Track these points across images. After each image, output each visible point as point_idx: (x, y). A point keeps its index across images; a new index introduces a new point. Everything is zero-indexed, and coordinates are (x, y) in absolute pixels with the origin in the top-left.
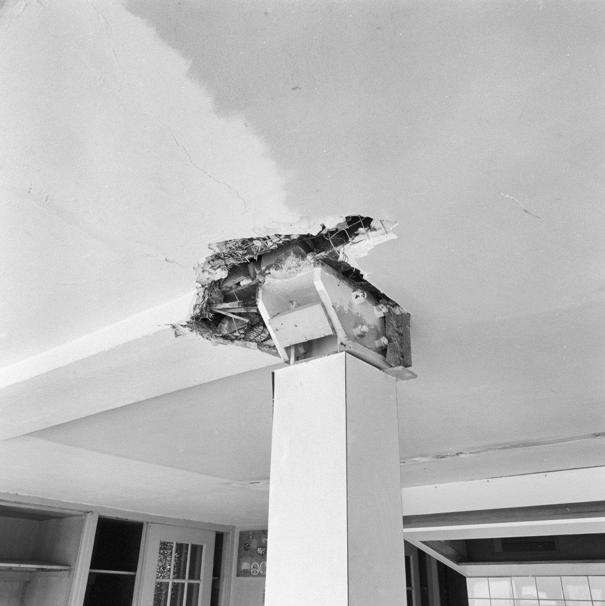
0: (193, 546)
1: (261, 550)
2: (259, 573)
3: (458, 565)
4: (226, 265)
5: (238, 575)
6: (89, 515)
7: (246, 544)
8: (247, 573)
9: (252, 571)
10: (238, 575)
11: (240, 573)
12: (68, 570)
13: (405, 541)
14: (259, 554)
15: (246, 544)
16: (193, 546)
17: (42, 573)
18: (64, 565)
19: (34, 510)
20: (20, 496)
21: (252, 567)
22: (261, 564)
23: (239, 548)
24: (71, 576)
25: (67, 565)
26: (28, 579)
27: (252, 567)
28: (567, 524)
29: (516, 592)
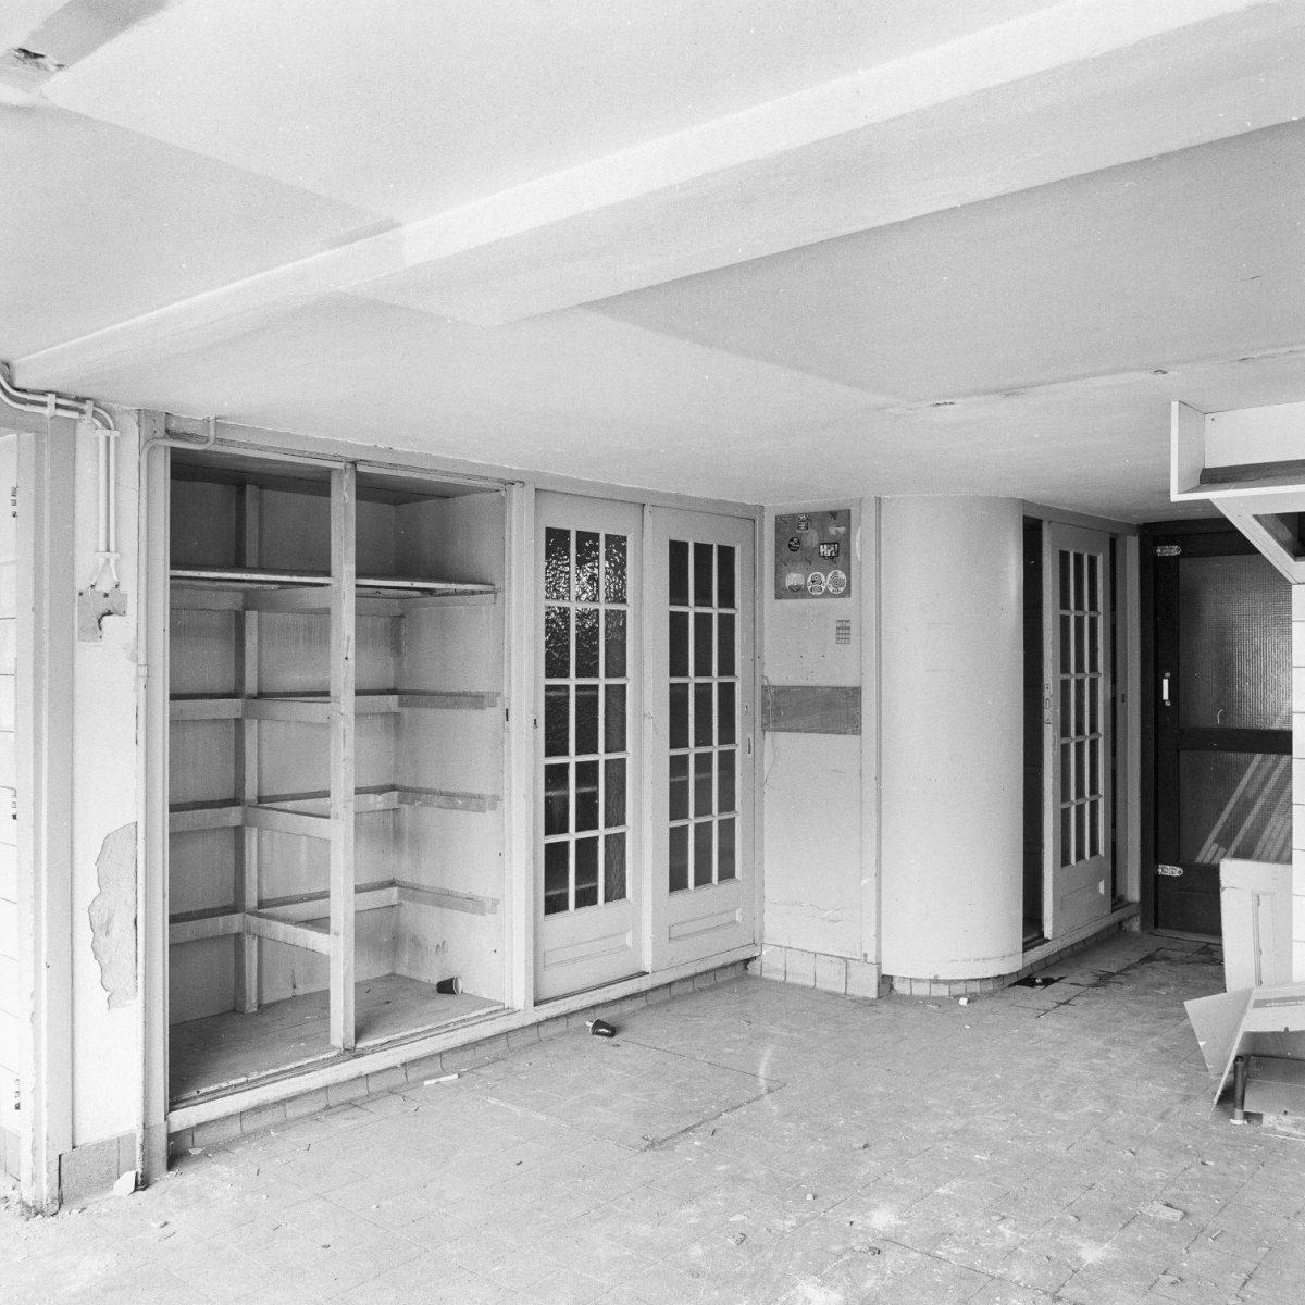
0: (697, 545)
1: (829, 548)
2: (827, 591)
3: (1295, 560)
4: (861, 911)
5: (778, 596)
6: (516, 489)
7: (792, 540)
8: (798, 592)
9: (809, 588)
10: (778, 596)
11: (782, 593)
12: (488, 592)
13: (1257, 517)
14: (824, 556)
15: (792, 540)
16: (697, 545)
17: (430, 599)
18: (475, 583)
19: (409, 480)
20: (397, 453)
21: (809, 580)
22: (830, 575)
23: (777, 548)
24: (499, 602)
25: (484, 583)
26: (398, 611)
27: (809, 580)
28: (696, 867)
29: (50, 728)
